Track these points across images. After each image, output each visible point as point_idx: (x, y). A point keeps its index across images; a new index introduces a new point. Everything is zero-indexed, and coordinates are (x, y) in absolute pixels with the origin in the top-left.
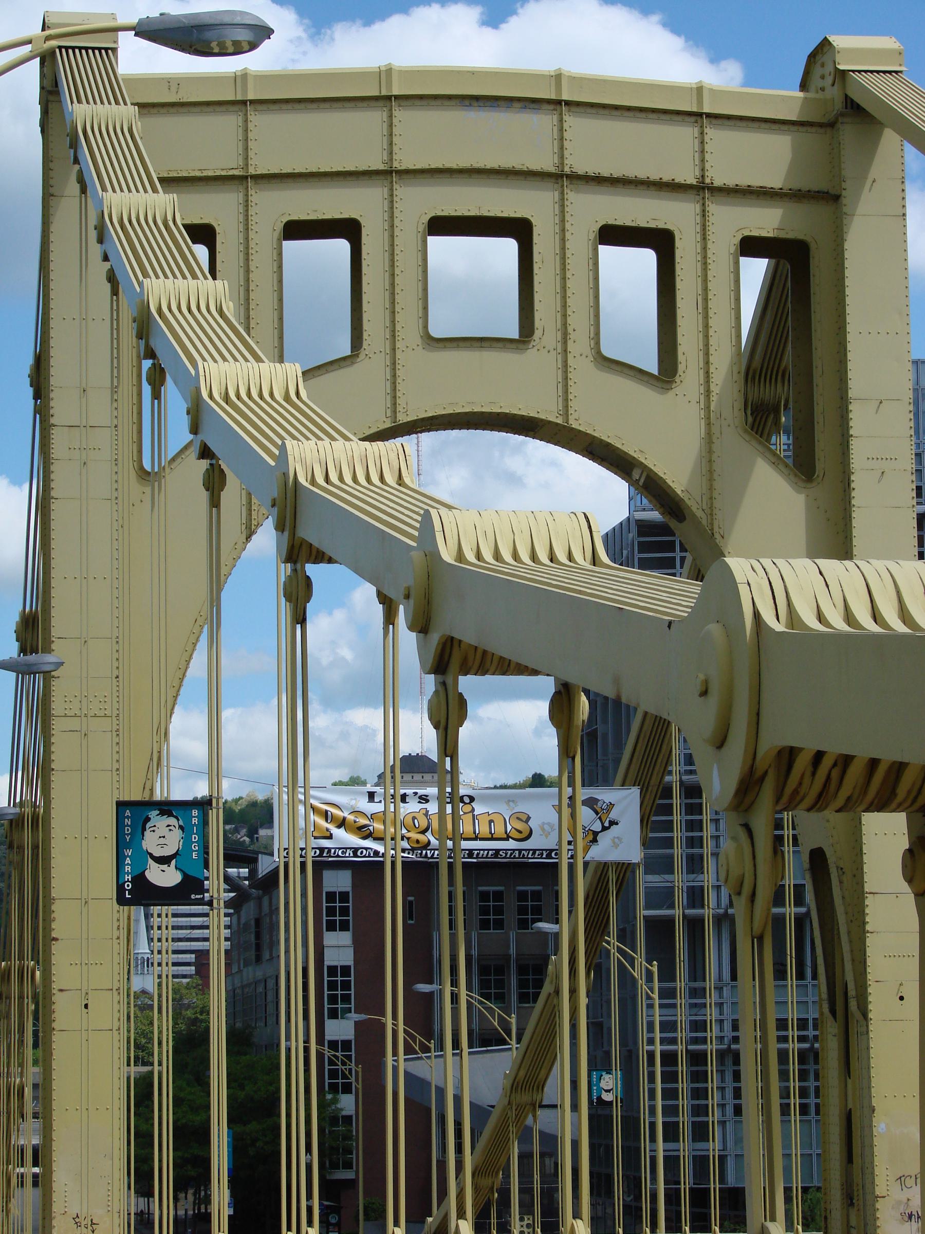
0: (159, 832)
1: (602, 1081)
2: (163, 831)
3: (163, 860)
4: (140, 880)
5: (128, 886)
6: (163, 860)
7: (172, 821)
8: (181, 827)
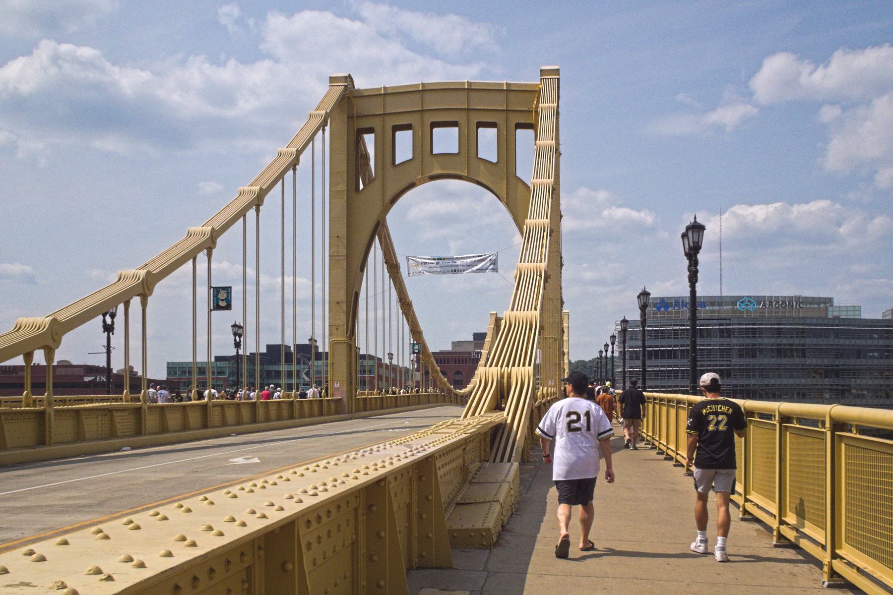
0: (223, 294)
1: (219, 294)
2: (223, 294)
3: (222, 300)
4: (414, 351)
5: (215, 306)
6: (222, 300)
7: (225, 291)
8: (227, 293)
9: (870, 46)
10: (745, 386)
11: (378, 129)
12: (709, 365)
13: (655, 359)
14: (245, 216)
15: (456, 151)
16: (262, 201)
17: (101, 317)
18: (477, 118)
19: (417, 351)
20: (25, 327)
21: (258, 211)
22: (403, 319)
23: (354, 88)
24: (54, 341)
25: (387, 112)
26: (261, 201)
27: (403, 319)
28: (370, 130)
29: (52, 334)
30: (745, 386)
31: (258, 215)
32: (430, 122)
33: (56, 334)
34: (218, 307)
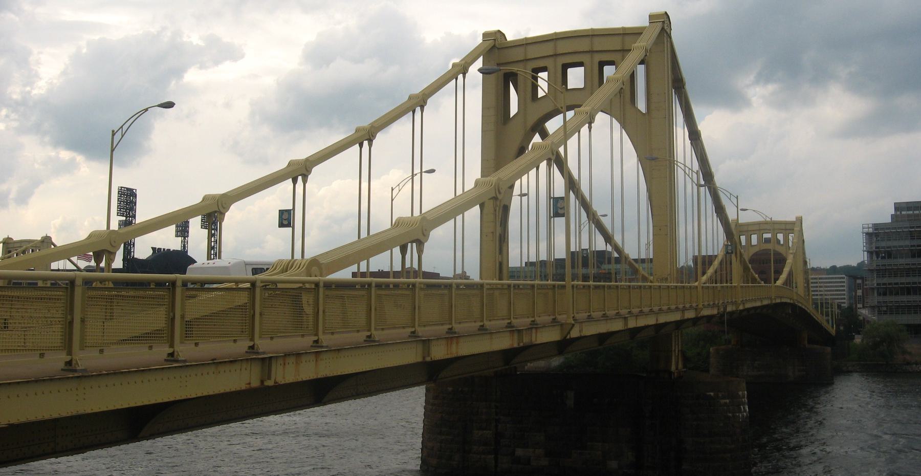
4: (728, 252)
9: (198, 65)
10: (391, 275)
11: (550, 67)
12: (611, 261)
13: (888, 258)
14: (579, 132)
15: (582, 86)
16: (594, 119)
17: (136, 223)
18: (598, 58)
19: (730, 251)
20: (402, 224)
21: (590, 128)
22: (717, 221)
23: (506, 40)
24: (424, 235)
25: (529, 57)
26: (593, 119)
27: (717, 221)
28: (544, 69)
29: (423, 231)
30: (391, 275)
31: (590, 131)
32: (561, 64)
33: (426, 230)
34: (288, 211)
